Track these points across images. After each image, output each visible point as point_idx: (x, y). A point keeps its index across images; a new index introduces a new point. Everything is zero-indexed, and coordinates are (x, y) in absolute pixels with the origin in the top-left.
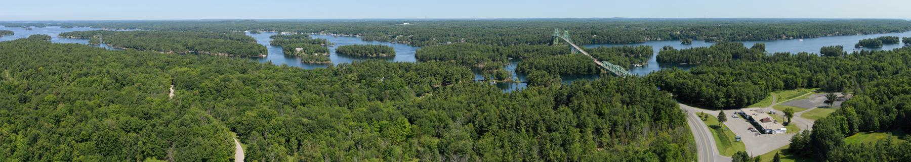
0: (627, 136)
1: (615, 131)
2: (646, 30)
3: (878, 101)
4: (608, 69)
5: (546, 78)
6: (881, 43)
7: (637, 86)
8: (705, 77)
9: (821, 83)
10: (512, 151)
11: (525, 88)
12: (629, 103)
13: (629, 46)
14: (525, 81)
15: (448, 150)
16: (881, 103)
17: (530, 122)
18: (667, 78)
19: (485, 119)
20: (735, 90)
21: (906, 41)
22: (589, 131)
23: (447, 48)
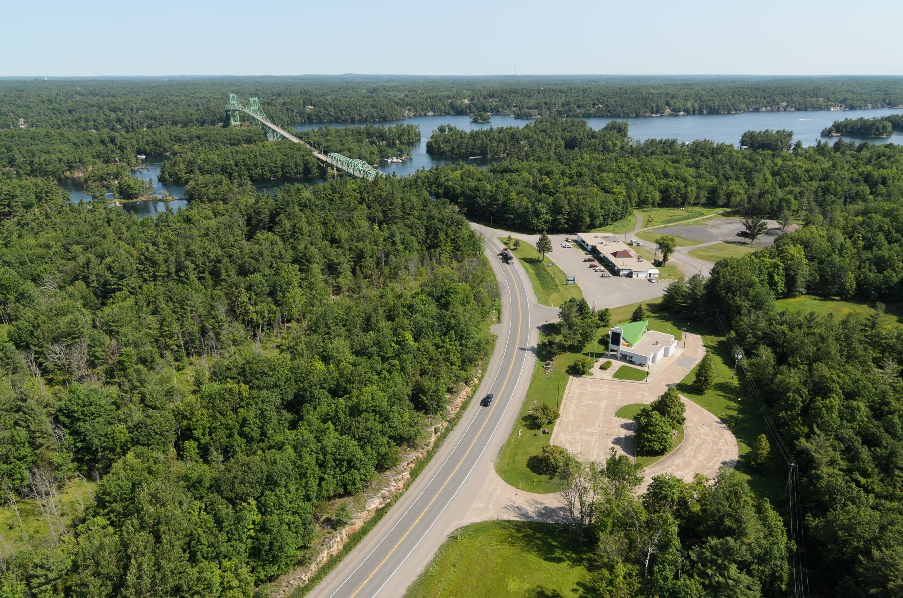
1: (361, 267)
2: (406, 96)
3: (862, 243)
4: (340, 166)
5: (224, 188)
6: (890, 129)
7: (396, 192)
8: (515, 176)
9: (736, 200)
10: (175, 316)
12: (385, 220)
15: (38, 338)
16: (868, 247)
17: (204, 264)
18: (448, 180)
19: (109, 268)
20: (570, 200)
22: (316, 268)
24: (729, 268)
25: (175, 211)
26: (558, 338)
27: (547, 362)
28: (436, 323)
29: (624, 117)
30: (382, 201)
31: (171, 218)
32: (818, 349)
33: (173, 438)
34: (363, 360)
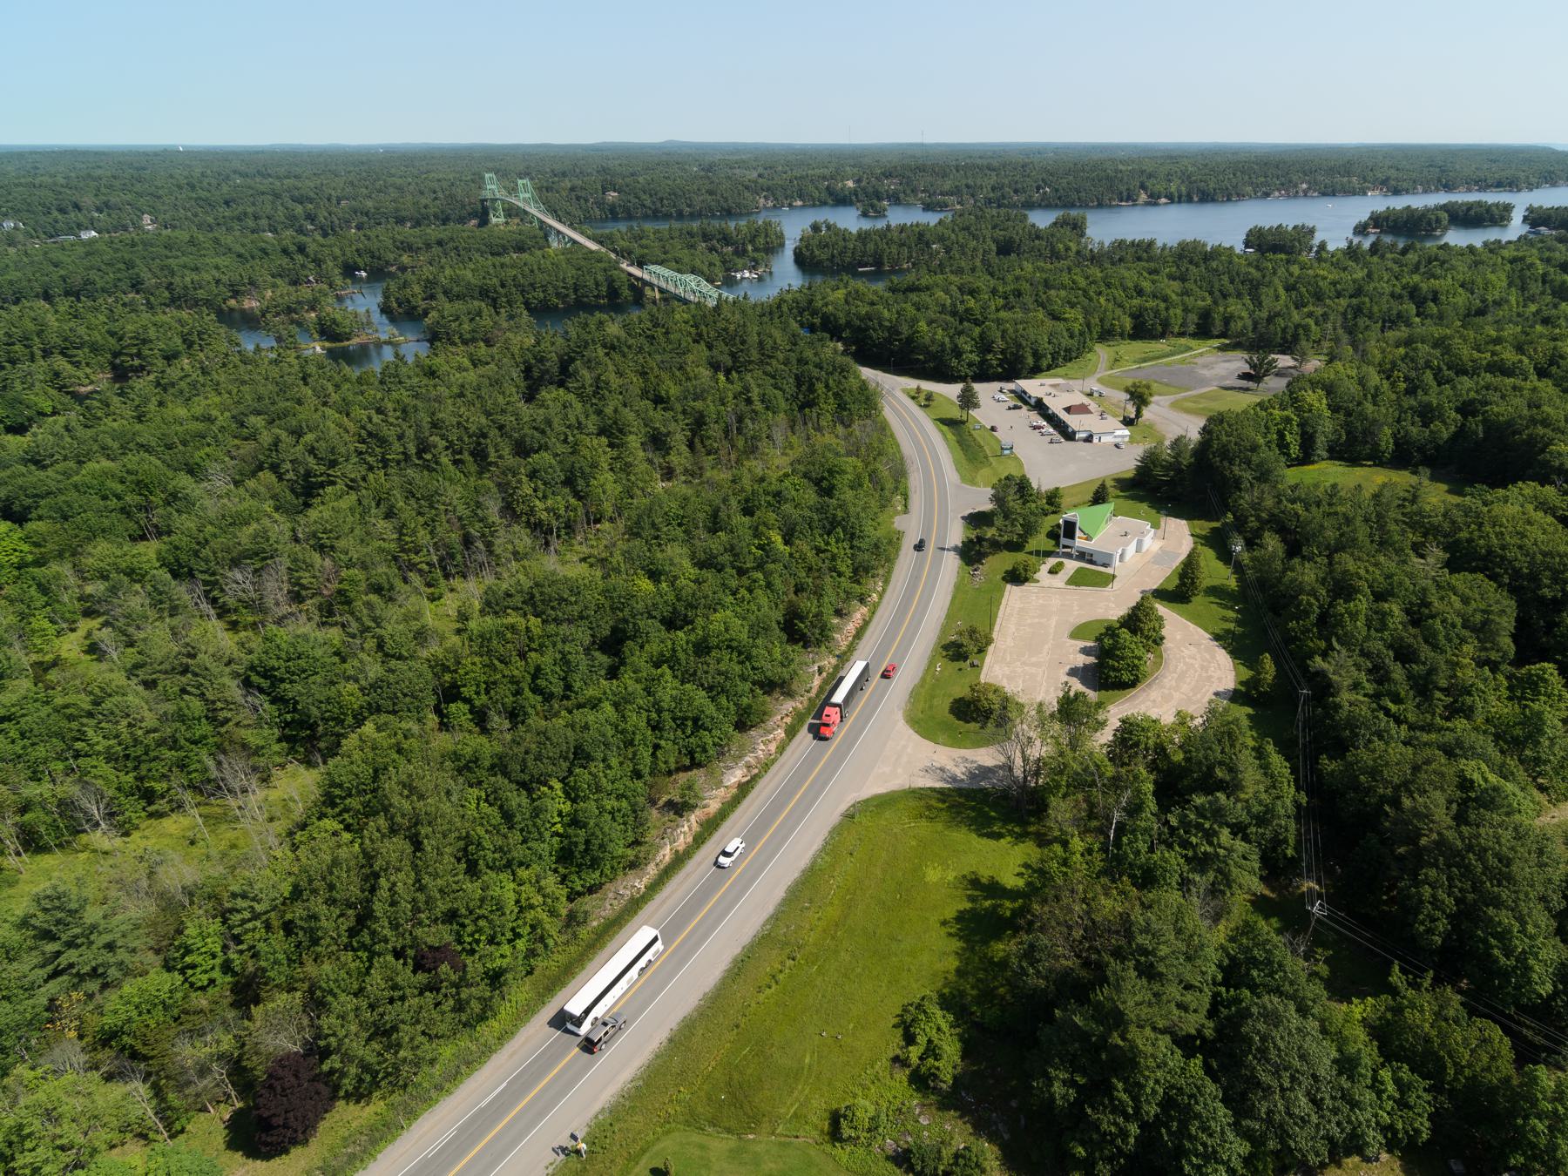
2: (760, 176)
3: (1402, 386)
4: (663, 285)
5: (486, 321)
8: (925, 297)
9: (1237, 326)
12: (734, 367)
13: (716, 223)
16: (1411, 391)
17: (460, 439)
18: (826, 305)
19: (312, 451)
20: (1004, 332)
21: (1535, 218)
22: (634, 441)
23: (88, 254)
25: (410, 360)
26: (990, 533)
30: (728, 337)
31: (404, 370)
32: (1342, 535)
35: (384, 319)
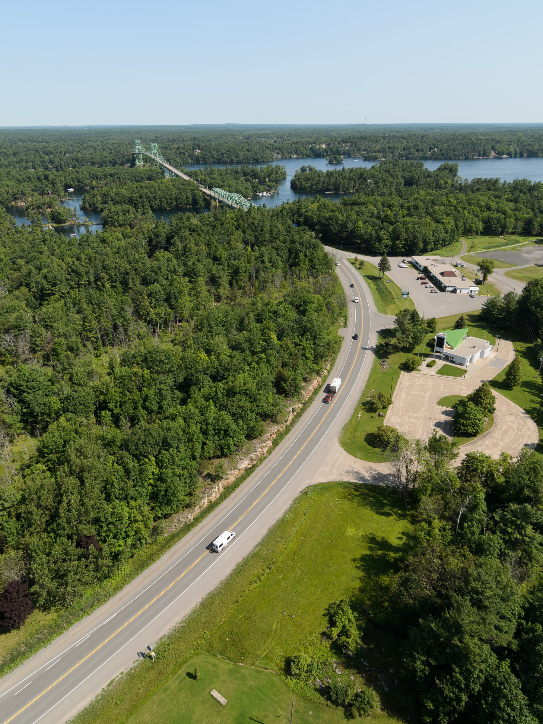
0: (253, 286)
2: (275, 142)
4: (221, 199)
5: (131, 215)
8: (362, 208)
10: (94, 315)
11: (100, 231)
13: (251, 167)
14: (99, 222)
17: (115, 275)
18: (307, 211)
19: (45, 277)
20: (407, 229)
22: (202, 280)
24: (539, 287)
25: (94, 233)
26: (393, 341)
27: (384, 359)
28: (295, 326)
29: (455, 159)
30: (254, 227)
31: (91, 239)
33: (93, 408)
34: (237, 354)
35: (82, 213)
